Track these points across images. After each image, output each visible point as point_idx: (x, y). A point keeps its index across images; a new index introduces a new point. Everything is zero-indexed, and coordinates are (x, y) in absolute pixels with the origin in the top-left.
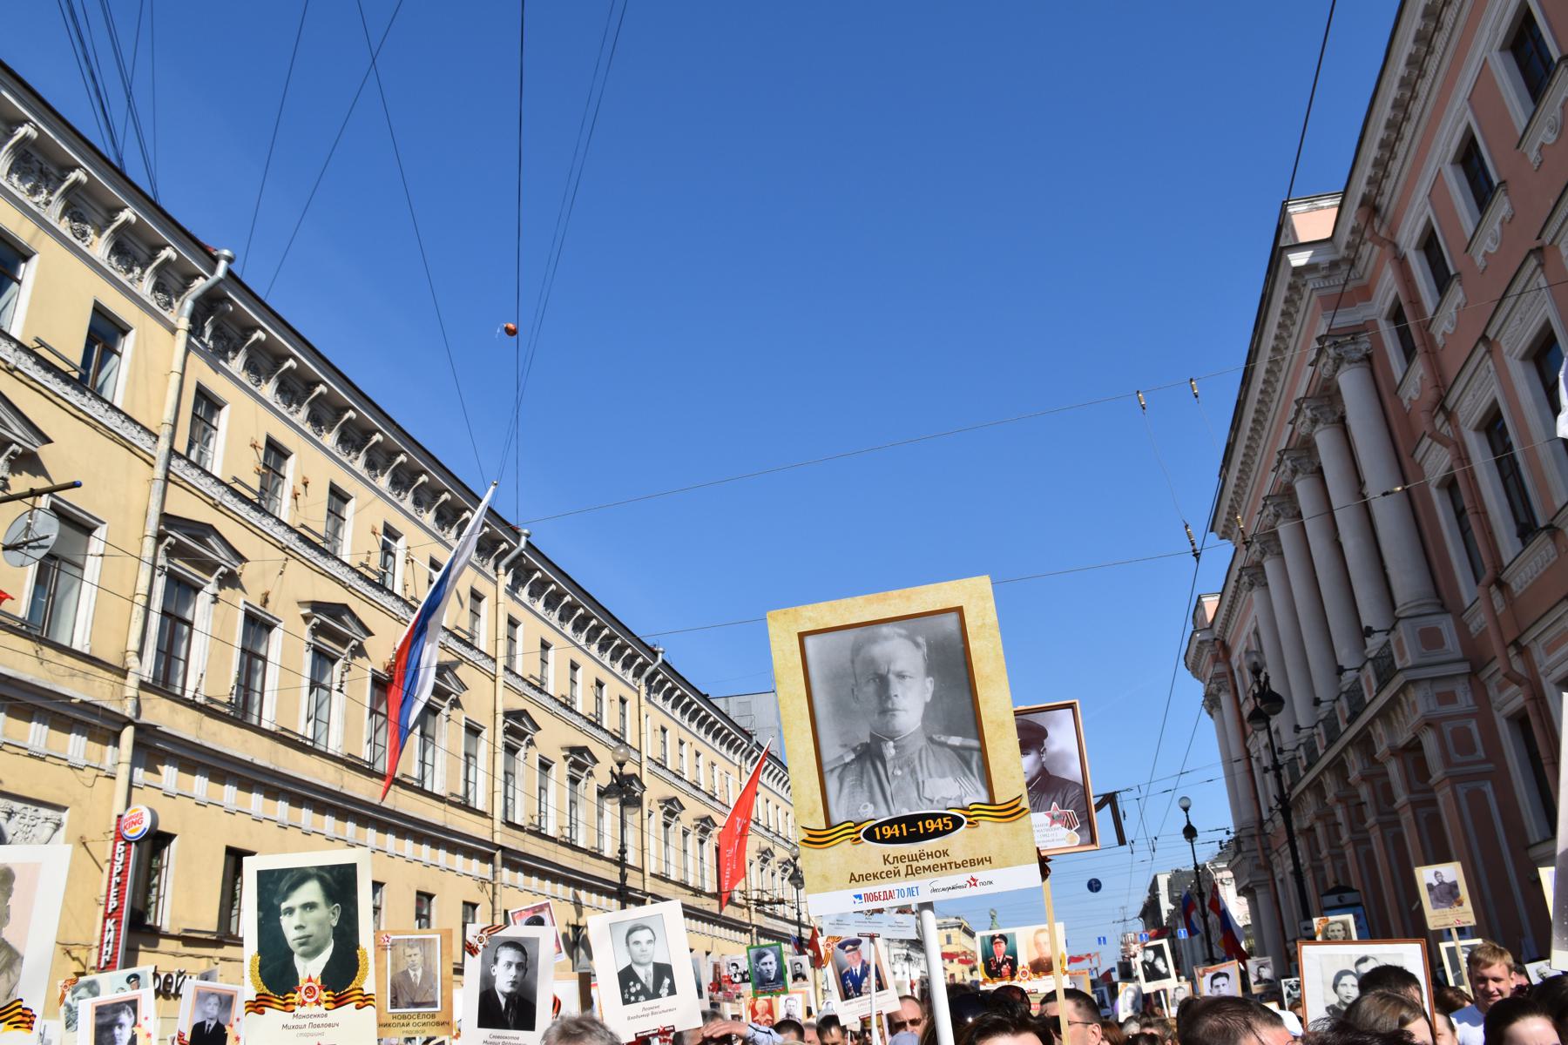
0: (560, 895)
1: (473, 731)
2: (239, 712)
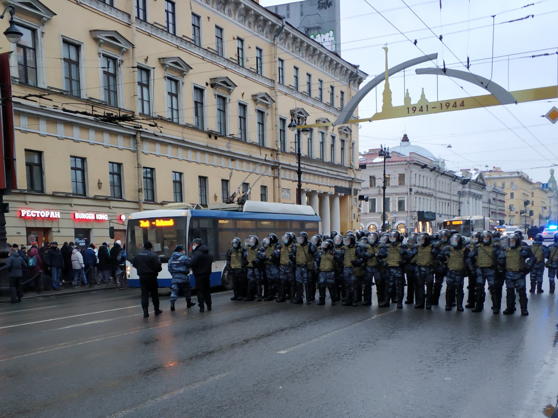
1: (199, 91)
2: (243, 140)
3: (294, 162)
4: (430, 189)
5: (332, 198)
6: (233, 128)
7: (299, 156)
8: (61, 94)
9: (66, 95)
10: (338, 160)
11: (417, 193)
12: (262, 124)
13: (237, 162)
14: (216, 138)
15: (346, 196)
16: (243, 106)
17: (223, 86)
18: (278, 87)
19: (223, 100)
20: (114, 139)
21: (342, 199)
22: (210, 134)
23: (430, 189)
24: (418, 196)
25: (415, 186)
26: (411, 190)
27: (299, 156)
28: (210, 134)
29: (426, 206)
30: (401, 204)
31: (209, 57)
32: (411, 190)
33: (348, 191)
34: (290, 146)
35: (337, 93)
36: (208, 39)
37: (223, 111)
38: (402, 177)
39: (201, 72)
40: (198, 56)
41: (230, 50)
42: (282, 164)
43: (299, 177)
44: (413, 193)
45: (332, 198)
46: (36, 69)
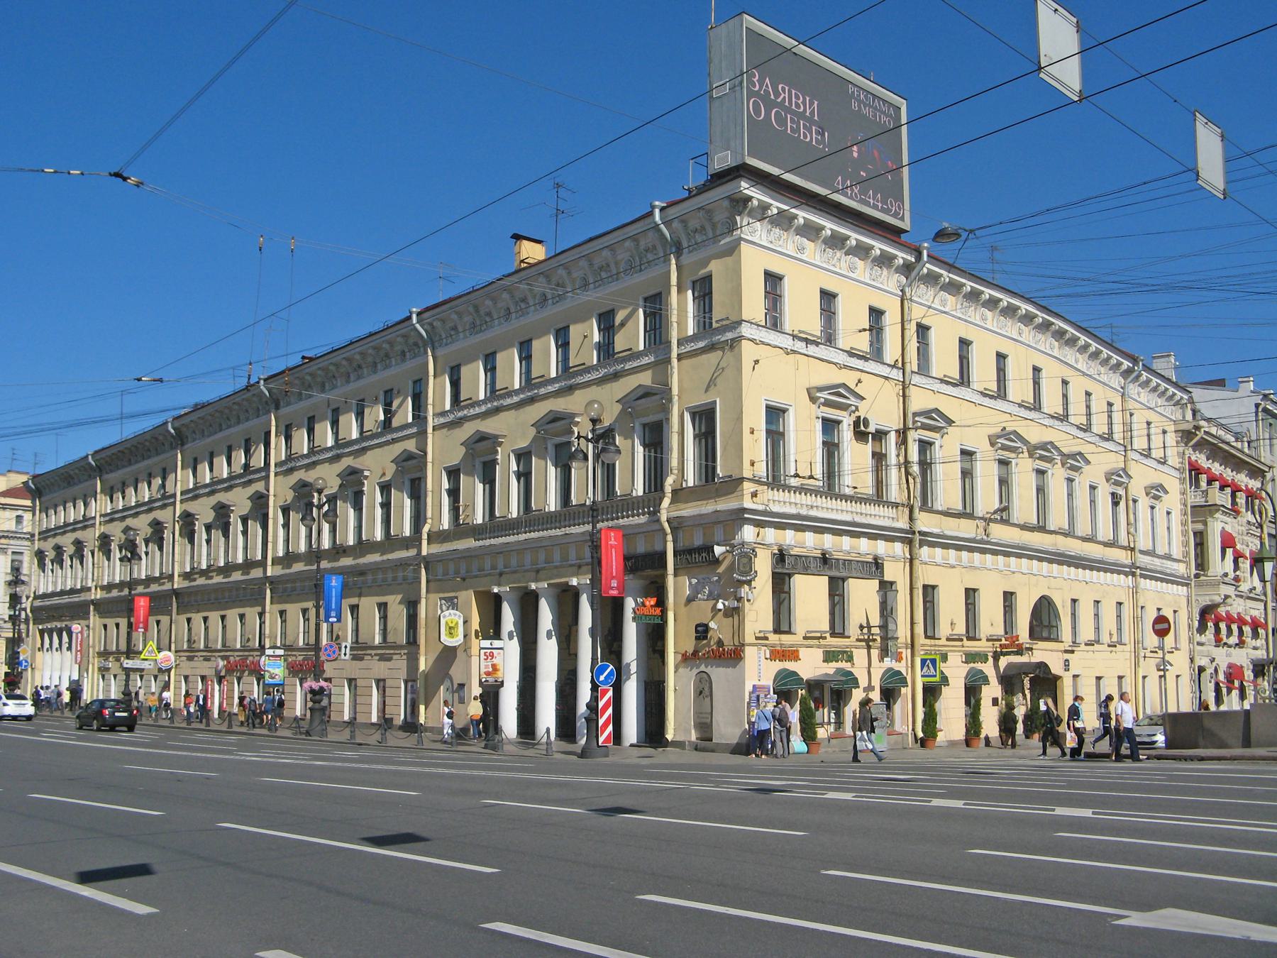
0: (989, 565)
1: (967, 454)
36: (984, 374)
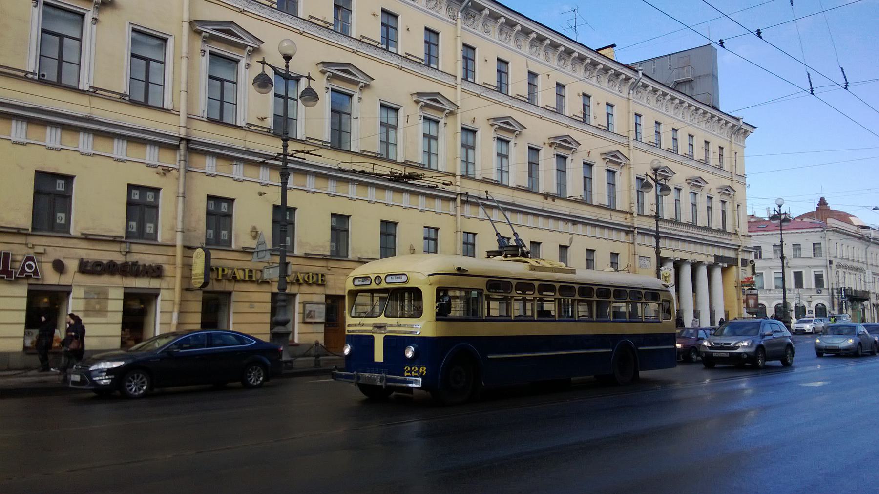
1: (147, 43)
2: (585, 202)
3: (651, 224)
4: (858, 261)
5: (710, 269)
6: (574, 188)
7: (657, 217)
8: (122, 98)
9: (32, 79)
10: (717, 224)
11: (839, 266)
12: (612, 185)
13: (580, 226)
14: (554, 200)
15: (730, 267)
16: (588, 166)
17: (564, 146)
18: (632, 144)
19: (562, 158)
20: (431, 201)
21: (724, 270)
22: (546, 196)
23: (858, 261)
24: (841, 271)
25: (836, 257)
26: (831, 262)
27: (657, 217)
28: (546, 196)
29: (852, 282)
30: (819, 280)
31: (547, 115)
32: (831, 262)
33: (733, 262)
34: (649, 208)
35: (713, 148)
37: (562, 171)
38: (816, 247)
39: (539, 129)
40: (533, 115)
41: (573, 106)
42: (638, 228)
43: (658, 243)
44: (834, 266)
45: (710, 269)
46: (79, 65)
